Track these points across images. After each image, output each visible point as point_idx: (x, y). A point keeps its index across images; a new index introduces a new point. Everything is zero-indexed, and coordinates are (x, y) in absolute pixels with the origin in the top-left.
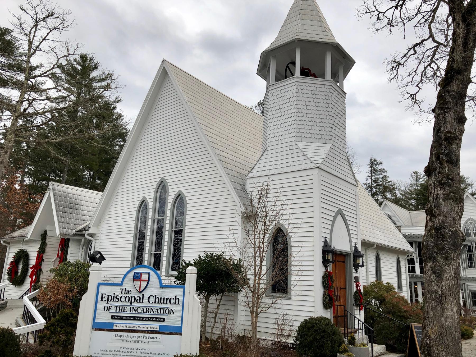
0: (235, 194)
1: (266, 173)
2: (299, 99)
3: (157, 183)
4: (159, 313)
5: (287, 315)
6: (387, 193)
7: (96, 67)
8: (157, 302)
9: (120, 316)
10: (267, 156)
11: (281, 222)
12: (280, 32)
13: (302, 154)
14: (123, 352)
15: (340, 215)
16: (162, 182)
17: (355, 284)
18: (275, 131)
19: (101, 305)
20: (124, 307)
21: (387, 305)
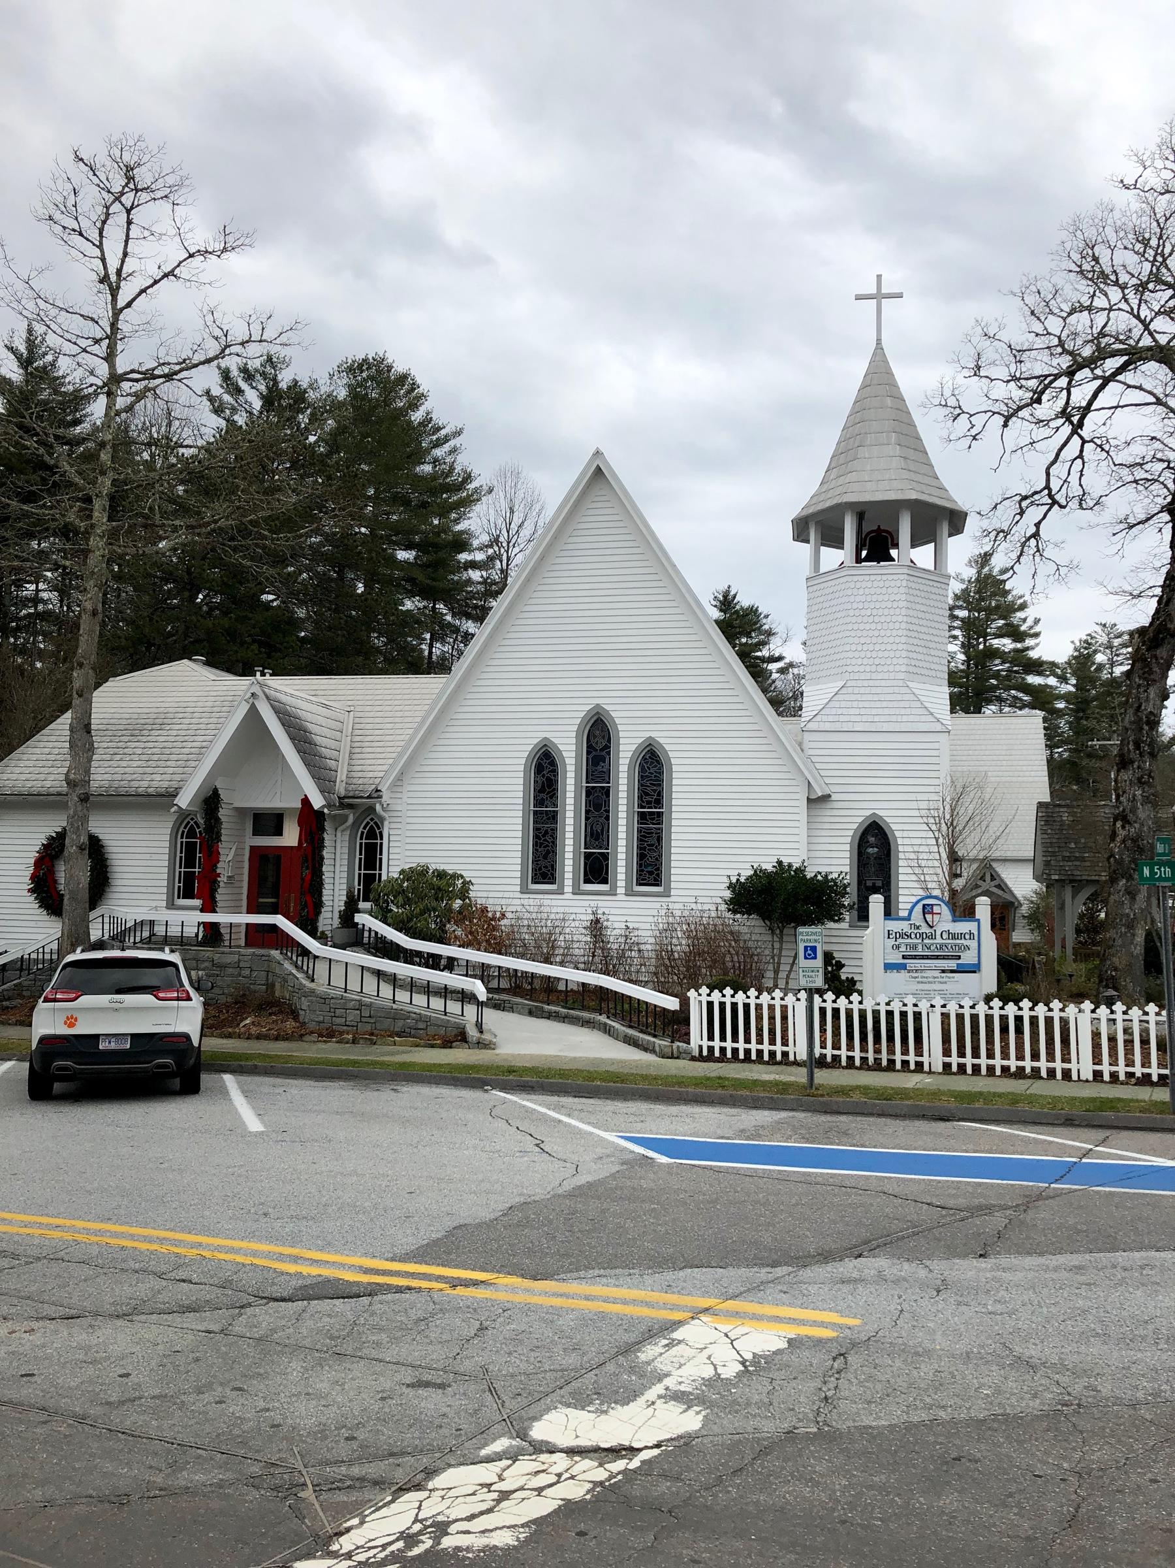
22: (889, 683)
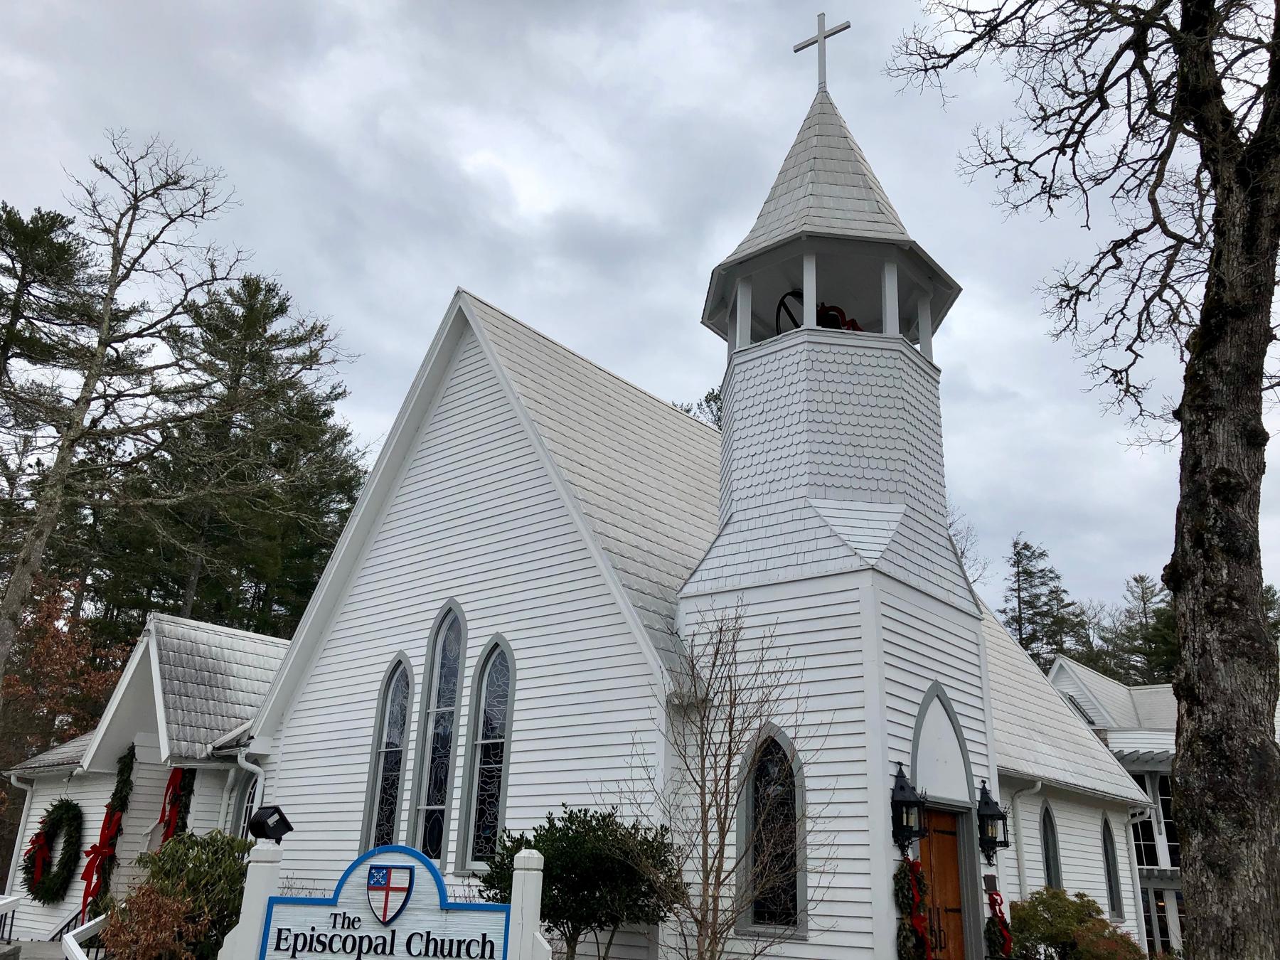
2: (815, 386)
7: (282, 310)
8: (431, 953)
10: (733, 539)
11: (776, 721)
13: (826, 532)
15: (936, 701)
16: (450, 610)
17: (986, 898)
22: (787, 506)
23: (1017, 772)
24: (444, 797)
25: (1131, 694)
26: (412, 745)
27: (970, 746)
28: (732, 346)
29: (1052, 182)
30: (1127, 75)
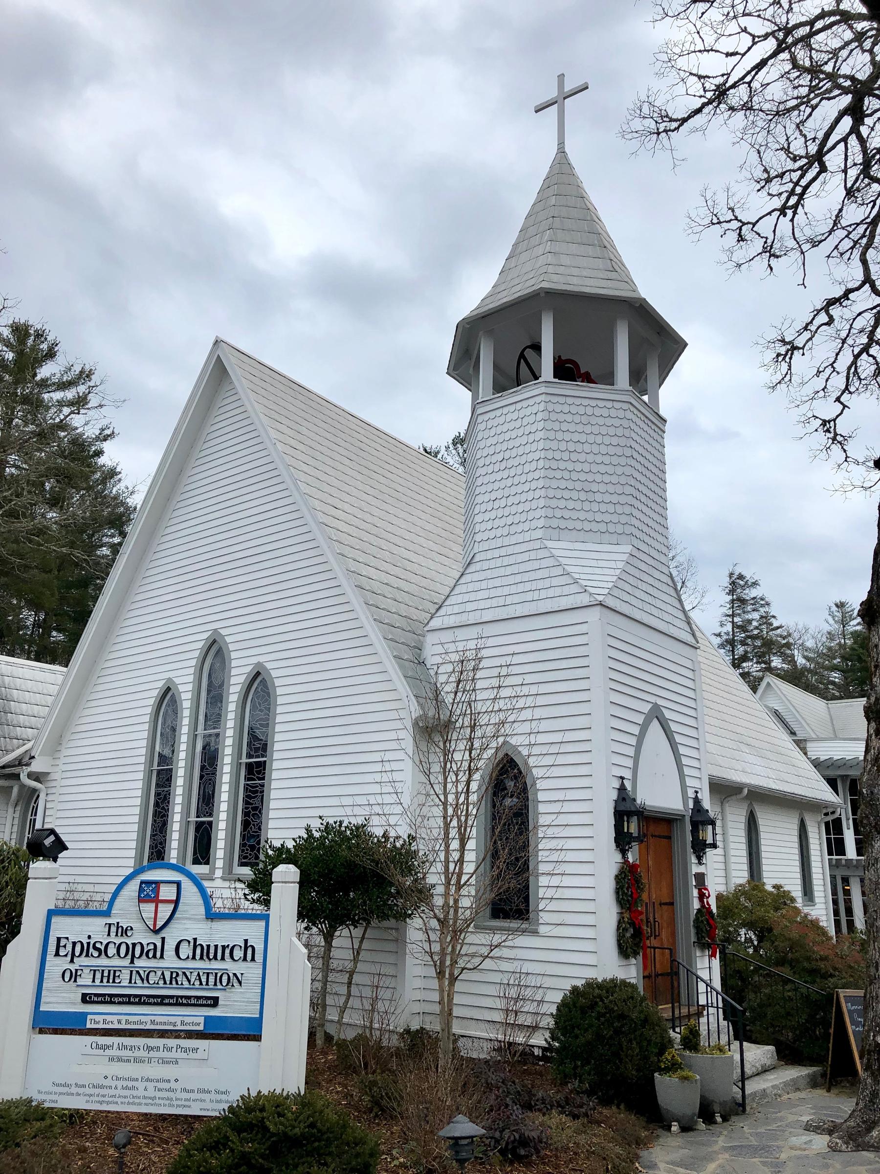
0: (395, 670)
1: (472, 618)
2: (551, 435)
3: (200, 645)
4: (204, 983)
5: (528, 974)
6: (771, 656)
7: (51, 354)
8: (198, 957)
9: (104, 995)
10: (476, 577)
11: (513, 741)
12: (502, 272)
13: (559, 571)
14: (110, 1087)
15: (655, 721)
16: (214, 641)
17: (695, 893)
18: (493, 515)
19: (56, 966)
20: (115, 971)
21: (776, 943)
22: (523, 548)
23: (727, 780)
24: (212, 810)
25: (828, 708)
26: (182, 764)
27: (685, 761)
28: (475, 397)
29: (773, 242)
30: (845, 140)
